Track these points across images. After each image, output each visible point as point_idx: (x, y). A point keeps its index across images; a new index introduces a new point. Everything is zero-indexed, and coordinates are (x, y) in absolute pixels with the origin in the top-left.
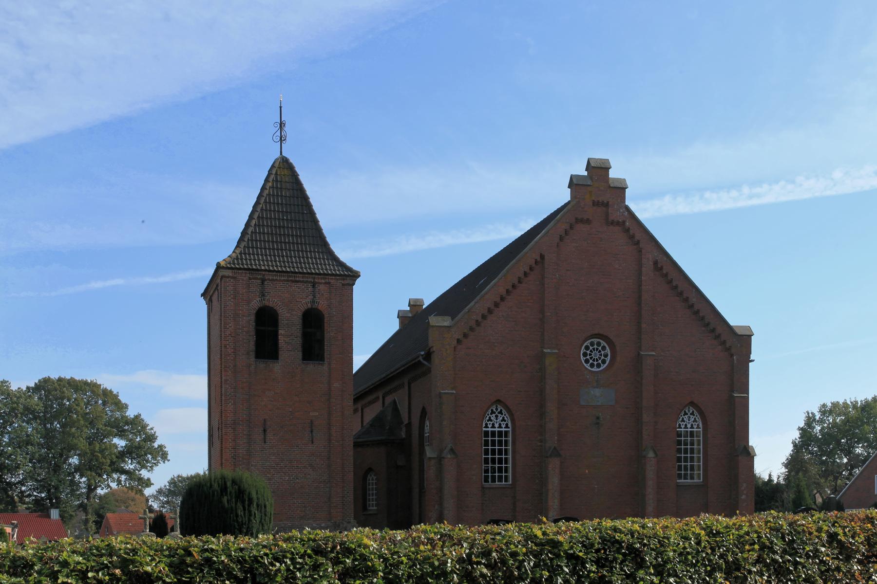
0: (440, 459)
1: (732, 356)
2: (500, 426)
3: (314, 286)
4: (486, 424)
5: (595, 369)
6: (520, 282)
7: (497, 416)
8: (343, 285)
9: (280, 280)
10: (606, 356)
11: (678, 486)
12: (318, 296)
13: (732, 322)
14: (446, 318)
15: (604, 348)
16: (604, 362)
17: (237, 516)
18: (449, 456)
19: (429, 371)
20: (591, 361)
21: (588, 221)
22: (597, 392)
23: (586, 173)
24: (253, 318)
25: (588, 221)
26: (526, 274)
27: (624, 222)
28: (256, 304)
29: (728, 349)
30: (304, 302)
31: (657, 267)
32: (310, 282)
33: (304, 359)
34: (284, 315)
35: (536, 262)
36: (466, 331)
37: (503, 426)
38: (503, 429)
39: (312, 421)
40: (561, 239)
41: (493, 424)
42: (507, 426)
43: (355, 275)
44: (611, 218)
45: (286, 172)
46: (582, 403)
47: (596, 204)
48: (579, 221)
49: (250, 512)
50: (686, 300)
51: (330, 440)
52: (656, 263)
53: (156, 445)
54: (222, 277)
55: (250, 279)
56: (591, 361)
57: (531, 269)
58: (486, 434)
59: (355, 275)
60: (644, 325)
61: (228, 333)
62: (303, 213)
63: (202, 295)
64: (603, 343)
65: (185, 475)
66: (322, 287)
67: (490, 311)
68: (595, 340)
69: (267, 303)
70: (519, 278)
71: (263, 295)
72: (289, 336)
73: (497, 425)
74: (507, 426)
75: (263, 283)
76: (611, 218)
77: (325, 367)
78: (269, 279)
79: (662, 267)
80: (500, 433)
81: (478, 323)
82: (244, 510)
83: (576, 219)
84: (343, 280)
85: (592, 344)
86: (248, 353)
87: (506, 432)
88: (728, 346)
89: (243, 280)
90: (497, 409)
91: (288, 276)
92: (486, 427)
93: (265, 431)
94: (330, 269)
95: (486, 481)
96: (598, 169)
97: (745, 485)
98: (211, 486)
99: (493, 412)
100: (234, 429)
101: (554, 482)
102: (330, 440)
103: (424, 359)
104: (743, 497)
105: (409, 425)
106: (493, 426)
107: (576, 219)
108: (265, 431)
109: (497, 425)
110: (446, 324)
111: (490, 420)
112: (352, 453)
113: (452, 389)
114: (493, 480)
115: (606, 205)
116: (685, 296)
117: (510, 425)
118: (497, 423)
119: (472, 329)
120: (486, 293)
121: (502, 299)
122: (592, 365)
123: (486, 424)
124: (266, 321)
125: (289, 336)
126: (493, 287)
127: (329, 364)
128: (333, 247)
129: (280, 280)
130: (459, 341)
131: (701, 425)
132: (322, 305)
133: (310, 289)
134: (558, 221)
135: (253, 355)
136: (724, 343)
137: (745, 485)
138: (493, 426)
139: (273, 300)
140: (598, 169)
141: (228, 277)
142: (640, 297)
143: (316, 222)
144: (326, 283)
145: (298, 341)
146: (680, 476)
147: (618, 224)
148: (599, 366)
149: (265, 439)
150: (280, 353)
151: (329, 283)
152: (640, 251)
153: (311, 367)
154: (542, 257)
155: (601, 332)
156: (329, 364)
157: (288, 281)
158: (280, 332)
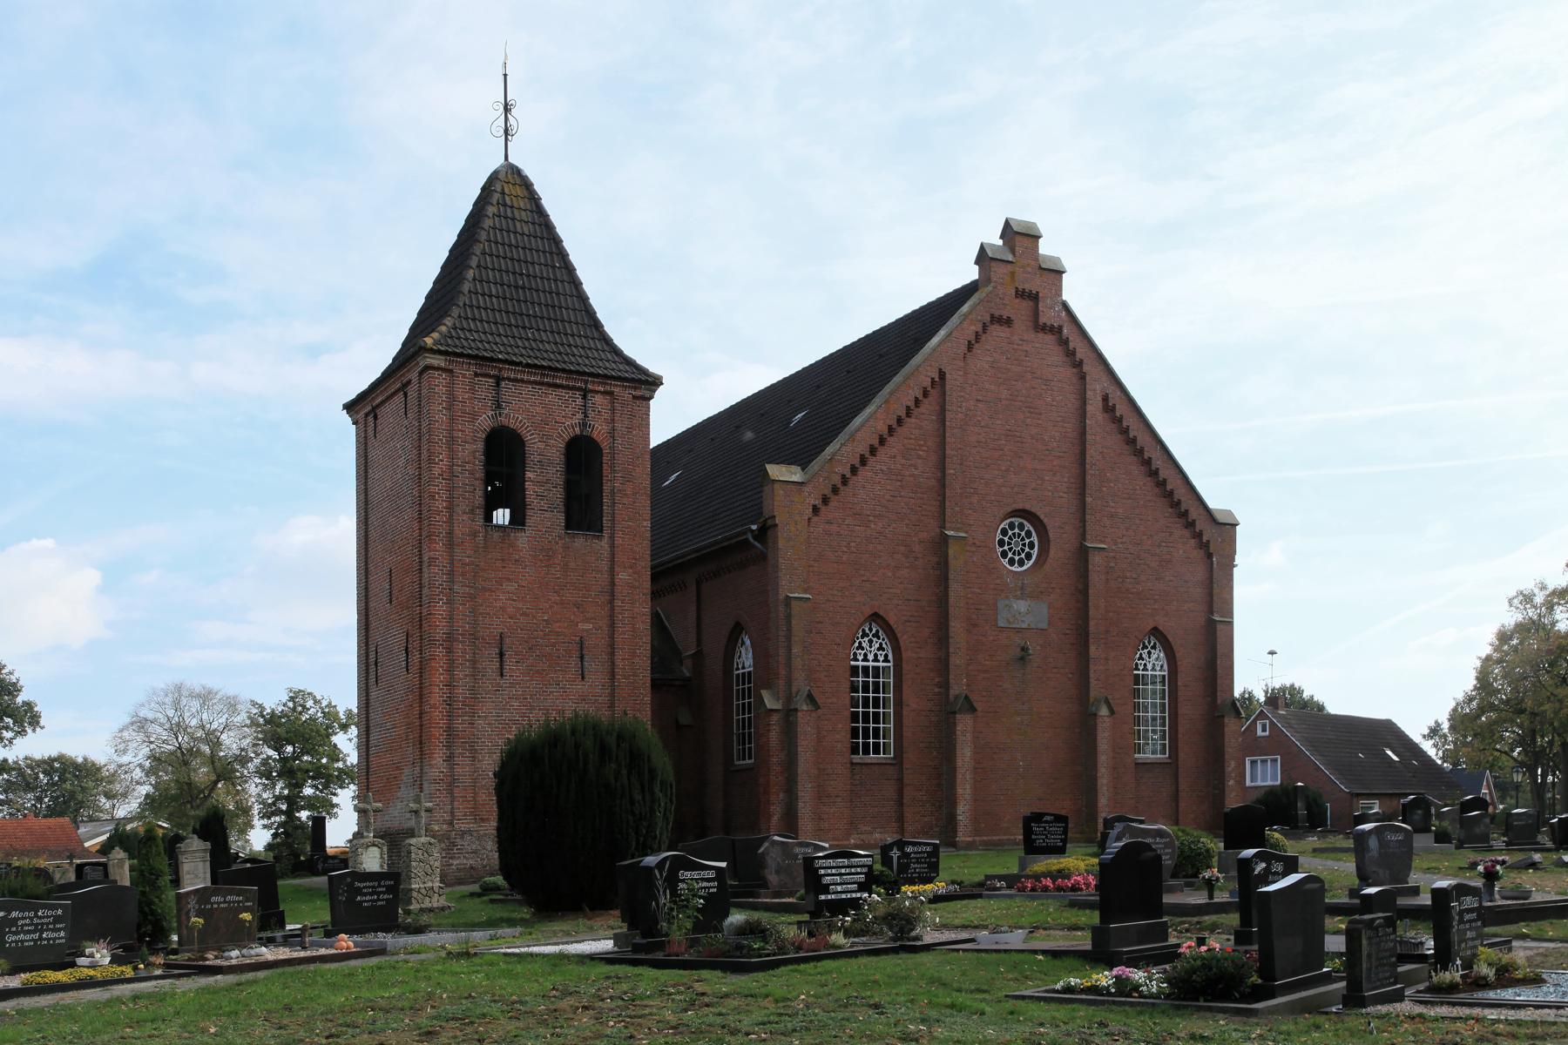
0: (789, 713)
2: (876, 659)
3: (584, 397)
5: (1015, 568)
6: (908, 415)
7: (871, 642)
8: (635, 397)
9: (529, 382)
10: (1032, 546)
12: (591, 414)
13: (1212, 504)
14: (794, 468)
15: (1029, 534)
16: (1029, 556)
17: (632, 802)
18: (805, 707)
19: (763, 557)
21: (1008, 322)
22: (1021, 606)
23: (1000, 242)
24: (480, 446)
25: (1008, 322)
26: (917, 401)
27: (1060, 327)
28: (485, 421)
31: (1108, 408)
32: (579, 389)
33: (568, 527)
38: (871, 664)
40: (970, 347)
43: (653, 382)
44: (1042, 320)
45: (519, 191)
46: (1001, 624)
47: (1021, 294)
49: (652, 794)
50: (1148, 462)
51: (613, 674)
52: (1105, 399)
53: (19, 700)
54: (428, 368)
55: (476, 375)
57: (925, 394)
58: (854, 671)
59: (653, 382)
60: (1089, 499)
61: (436, 471)
62: (554, 267)
63: (350, 407)
64: (1028, 526)
65: (38, 756)
66: (598, 398)
68: (1017, 521)
69: (503, 420)
70: (908, 408)
71: (499, 407)
72: (544, 480)
73: (871, 657)
75: (498, 385)
76: (1042, 320)
77: (605, 543)
78: (509, 379)
81: (845, 480)
82: (643, 790)
83: (992, 316)
85: (1012, 526)
86: (472, 512)
89: (464, 376)
93: (501, 655)
94: (612, 368)
95: (855, 750)
96: (1019, 237)
98: (577, 746)
99: (865, 635)
100: (449, 650)
101: (965, 755)
102: (613, 674)
103: (755, 538)
105: (698, 656)
106: (865, 659)
107: (992, 316)
108: (501, 655)
109: (871, 657)
110: (795, 478)
112: (648, 699)
113: (806, 591)
114: (866, 752)
115: (1034, 297)
116: (827, 492)
117: (890, 657)
118: (872, 653)
119: (835, 490)
120: (858, 430)
125: (544, 480)
126: (868, 420)
127: (612, 537)
128: (609, 328)
129: (529, 382)
130: (816, 510)
132: (599, 431)
133: (579, 401)
134: (966, 316)
136: (1199, 535)
138: (865, 659)
140: (1019, 237)
141: (438, 369)
142: (1083, 453)
143: (576, 284)
144: (605, 393)
145: (557, 494)
148: (1021, 563)
150: (529, 513)
153: (580, 542)
154: (942, 375)
155: (1027, 507)
156: (612, 537)
158: (528, 474)
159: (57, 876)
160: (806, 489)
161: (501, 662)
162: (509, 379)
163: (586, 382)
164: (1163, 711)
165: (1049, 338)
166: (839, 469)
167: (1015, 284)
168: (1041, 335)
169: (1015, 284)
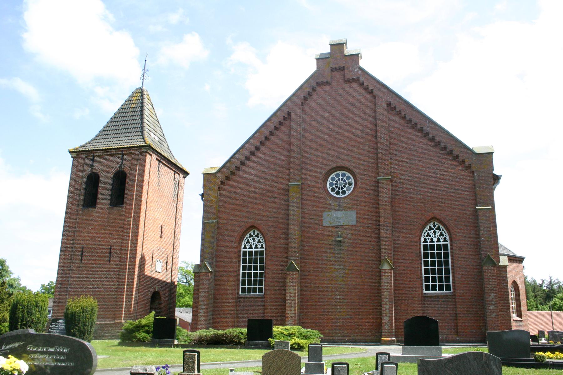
1: (473, 173)
2: (256, 247)
3: (123, 157)
4: (245, 246)
8: (141, 153)
11: (425, 297)
20: (337, 190)
21: (328, 83)
22: (339, 214)
25: (328, 83)
27: (358, 79)
28: (88, 172)
29: (469, 167)
30: (115, 168)
34: (103, 176)
35: (285, 119)
36: (227, 175)
37: (442, 240)
39: (111, 246)
41: (251, 246)
42: (445, 240)
46: (325, 224)
48: (319, 84)
52: (389, 105)
55: (86, 157)
56: (337, 190)
60: (380, 155)
67: (248, 159)
73: (253, 246)
74: (445, 240)
79: (395, 107)
80: (439, 247)
83: (317, 83)
84: (140, 149)
87: (446, 247)
88: (467, 164)
90: (254, 233)
91: (107, 152)
92: (245, 247)
93: (82, 254)
97: (493, 295)
104: (491, 307)
106: (251, 247)
107: (317, 83)
108: (82, 254)
109: (253, 246)
111: (248, 242)
114: (249, 291)
117: (448, 239)
118: (434, 236)
121: (257, 148)
122: (338, 193)
123: (256, 245)
124: (93, 181)
130: (222, 183)
131: (448, 239)
135: (81, 204)
137: (493, 295)
138: (251, 247)
139: (97, 169)
146: (427, 288)
147: (354, 80)
149: (81, 259)
150: (98, 201)
151: (131, 153)
152: (375, 98)
154: (289, 114)
157: (107, 155)
159: (74, 308)
160: (217, 175)
161: (82, 257)
162: (99, 156)
163: (122, 151)
164: (295, 308)
165: (354, 85)
166: (234, 165)
167: (339, 70)
168: (348, 84)
169: (339, 70)
